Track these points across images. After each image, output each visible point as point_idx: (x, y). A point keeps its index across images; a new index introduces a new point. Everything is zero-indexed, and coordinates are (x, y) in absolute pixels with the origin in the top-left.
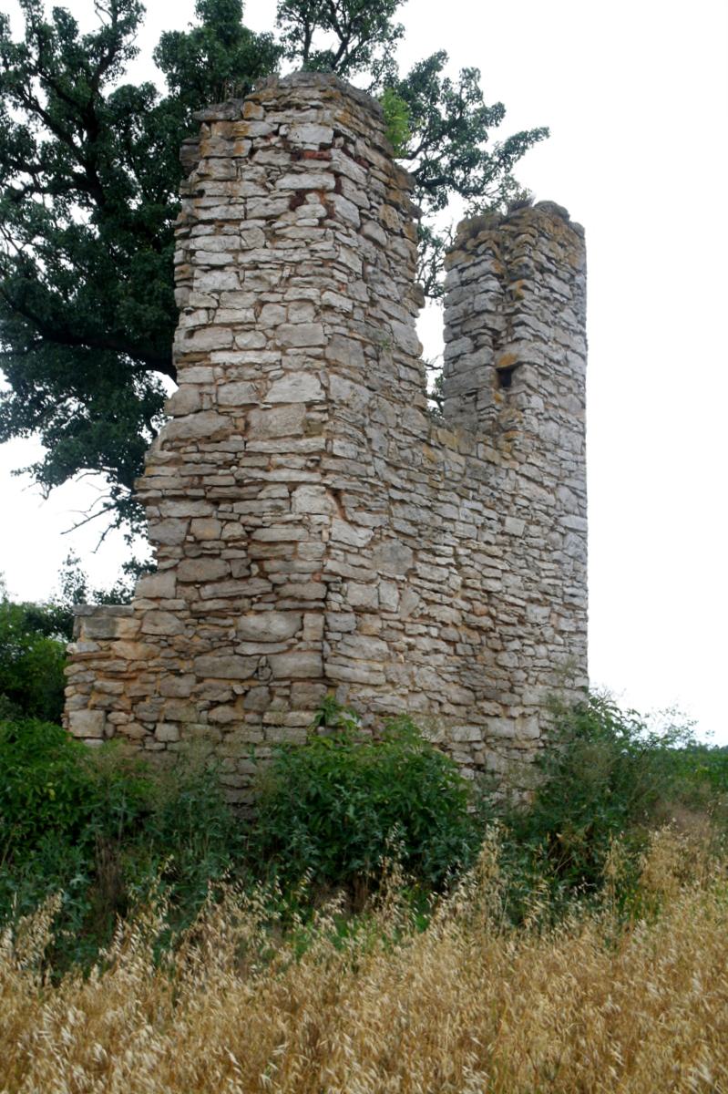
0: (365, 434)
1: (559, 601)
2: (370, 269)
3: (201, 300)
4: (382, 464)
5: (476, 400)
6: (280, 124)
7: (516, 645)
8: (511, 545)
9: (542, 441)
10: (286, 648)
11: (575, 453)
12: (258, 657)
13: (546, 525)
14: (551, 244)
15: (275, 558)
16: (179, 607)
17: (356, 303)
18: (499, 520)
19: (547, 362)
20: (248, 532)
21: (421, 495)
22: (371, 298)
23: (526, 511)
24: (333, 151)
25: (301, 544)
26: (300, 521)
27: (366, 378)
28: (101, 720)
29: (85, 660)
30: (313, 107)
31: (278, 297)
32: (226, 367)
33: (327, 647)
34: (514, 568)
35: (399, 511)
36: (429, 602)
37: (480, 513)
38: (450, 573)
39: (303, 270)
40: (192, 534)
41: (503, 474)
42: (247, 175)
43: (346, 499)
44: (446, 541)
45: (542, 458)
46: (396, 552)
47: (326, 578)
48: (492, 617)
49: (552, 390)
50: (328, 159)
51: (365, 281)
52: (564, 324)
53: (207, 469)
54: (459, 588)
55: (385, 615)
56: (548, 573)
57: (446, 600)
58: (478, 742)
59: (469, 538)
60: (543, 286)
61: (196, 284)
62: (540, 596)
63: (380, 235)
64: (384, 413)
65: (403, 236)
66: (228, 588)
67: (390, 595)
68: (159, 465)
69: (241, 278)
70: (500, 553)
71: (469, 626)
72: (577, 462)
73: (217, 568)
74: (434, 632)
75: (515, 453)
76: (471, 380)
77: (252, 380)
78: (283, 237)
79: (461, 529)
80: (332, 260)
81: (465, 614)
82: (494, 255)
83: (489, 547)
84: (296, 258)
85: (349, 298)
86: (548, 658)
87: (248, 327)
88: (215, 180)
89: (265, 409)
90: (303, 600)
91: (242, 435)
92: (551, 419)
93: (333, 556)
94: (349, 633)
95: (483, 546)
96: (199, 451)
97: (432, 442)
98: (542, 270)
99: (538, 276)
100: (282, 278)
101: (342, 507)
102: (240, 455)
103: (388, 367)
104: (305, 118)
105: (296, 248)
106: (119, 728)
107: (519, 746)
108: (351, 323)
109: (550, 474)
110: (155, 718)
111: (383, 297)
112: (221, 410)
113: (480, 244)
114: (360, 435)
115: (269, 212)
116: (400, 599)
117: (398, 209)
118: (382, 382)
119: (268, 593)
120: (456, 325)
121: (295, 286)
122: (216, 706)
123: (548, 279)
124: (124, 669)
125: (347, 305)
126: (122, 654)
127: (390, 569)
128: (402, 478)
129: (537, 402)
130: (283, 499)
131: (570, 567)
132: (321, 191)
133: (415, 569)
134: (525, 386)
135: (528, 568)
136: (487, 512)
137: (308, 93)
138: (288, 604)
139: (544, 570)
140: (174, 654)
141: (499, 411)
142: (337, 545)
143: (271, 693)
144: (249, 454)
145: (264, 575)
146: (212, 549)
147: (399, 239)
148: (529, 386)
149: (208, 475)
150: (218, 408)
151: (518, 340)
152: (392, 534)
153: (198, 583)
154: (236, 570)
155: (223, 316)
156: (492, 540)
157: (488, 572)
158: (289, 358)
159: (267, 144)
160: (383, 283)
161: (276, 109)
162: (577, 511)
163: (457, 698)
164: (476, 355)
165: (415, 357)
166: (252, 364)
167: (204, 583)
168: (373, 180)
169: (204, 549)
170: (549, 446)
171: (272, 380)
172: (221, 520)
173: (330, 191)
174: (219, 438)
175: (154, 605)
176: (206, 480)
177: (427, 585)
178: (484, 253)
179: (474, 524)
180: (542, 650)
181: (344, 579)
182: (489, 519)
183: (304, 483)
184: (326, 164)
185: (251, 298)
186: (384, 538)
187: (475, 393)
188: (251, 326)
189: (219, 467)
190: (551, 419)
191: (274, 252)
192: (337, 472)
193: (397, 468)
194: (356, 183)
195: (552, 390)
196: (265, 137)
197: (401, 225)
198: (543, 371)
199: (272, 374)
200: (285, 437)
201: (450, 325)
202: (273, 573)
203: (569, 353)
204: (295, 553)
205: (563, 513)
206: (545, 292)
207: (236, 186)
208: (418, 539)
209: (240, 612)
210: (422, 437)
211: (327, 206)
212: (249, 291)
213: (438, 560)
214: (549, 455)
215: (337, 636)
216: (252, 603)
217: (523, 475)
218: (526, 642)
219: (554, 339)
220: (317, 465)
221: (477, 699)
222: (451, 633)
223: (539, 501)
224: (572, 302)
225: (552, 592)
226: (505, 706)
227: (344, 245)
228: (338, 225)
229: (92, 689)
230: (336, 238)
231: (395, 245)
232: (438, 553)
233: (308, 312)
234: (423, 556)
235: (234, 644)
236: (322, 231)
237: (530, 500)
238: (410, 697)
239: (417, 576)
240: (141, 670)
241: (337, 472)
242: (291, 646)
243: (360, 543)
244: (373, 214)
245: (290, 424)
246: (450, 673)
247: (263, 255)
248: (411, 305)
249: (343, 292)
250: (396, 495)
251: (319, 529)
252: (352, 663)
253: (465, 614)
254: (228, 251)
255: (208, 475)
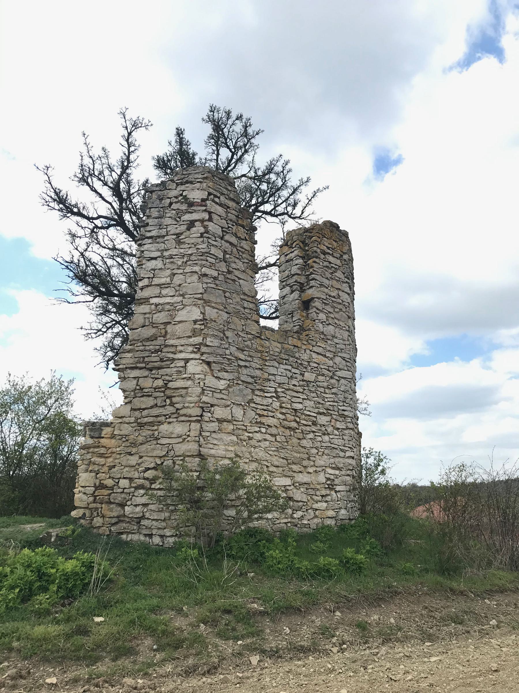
0: (224, 334)
1: (336, 413)
2: (228, 256)
3: (146, 274)
4: (235, 348)
5: (292, 317)
6: (183, 191)
7: (311, 436)
8: (308, 386)
9: (325, 335)
10: (182, 440)
11: (344, 340)
12: (168, 445)
13: (328, 376)
14: (329, 241)
15: (178, 396)
16: (131, 421)
17: (220, 273)
18: (301, 374)
19: (328, 297)
20: (166, 384)
21: (256, 363)
22: (228, 270)
23: (316, 369)
24: (207, 202)
25: (190, 389)
26: (190, 377)
27: (225, 308)
28: (94, 478)
29: (88, 448)
30: (198, 182)
31: (181, 271)
32: (156, 305)
33: (201, 439)
34: (309, 397)
35: (245, 371)
36: (260, 416)
37: (290, 371)
38: (273, 400)
39: (193, 258)
40: (139, 386)
41: (303, 352)
42: (168, 215)
43: (214, 366)
44: (270, 385)
45: (325, 343)
46: (242, 392)
47: (201, 405)
48: (297, 422)
49: (331, 310)
50: (206, 206)
51: (226, 262)
52: (337, 278)
53: (147, 354)
54: (278, 408)
55: (235, 423)
56: (329, 399)
57: (270, 414)
58: (290, 486)
59: (283, 383)
60: (325, 261)
61: (144, 266)
62: (325, 411)
63: (233, 240)
64: (235, 324)
65: (246, 240)
66: (156, 411)
67: (238, 413)
68: (125, 353)
69: (165, 263)
70: (301, 390)
71: (284, 427)
72: (345, 345)
73: (150, 401)
74: (263, 430)
75: (310, 341)
76: (290, 307)
77: (168, 311)
78: (184, 243)
79: (278, 379)
80: (206, 253)
81: (281, 421)
82: (300, 248)
83: (295, 388)
84: (190, 252)
85: (216, 270)
86: (330, 442)
87: (167, 286)
88: (153, 218)
89: (174, 324)
90: (190, 416)
91: (164, 337)
92: (330, 324)
93: (206, 394)
94: (214, 432)
95: (292, 387)
96: (143, 346)
97: (263, 337)
98: (324, 253)
99: (322, 256)
100: (183, 262)
101: (212, 370)
102: (162, 347)
103: (237, 302)
104: (195, 187)
105: (190, 248)
106: (102, 482)
107: (313, 487)
108: (217, 282)
109: (329, 351)
110: (119, 477)
111: (235, 269)
112: (154, 325)
113: (294, 242)
114: (222, 335)
115: (178, 232)
116: (244, 414)
117: (244, 228)
118: (234, 310)
119: (174, 413)
120: (284, 281)
121: (190, 265)
122: (148, 470)
123: (328, 258)
124: (105, 452)
125: (215, 274)
126: (105, 445)
127: (239, 400)
128: (245, 355)
129: (322, 316)
130: (182, 367)
131: (342, 396)
132: (202, 221)
133: (253, 399)
134: (315, 309)
135: (318, 397)
136: (293, 370)
137: (197, 176)
138: (183, 418)
139: (327, 398)
140: (129, 444)
141: (303, 321)
142: (208, 389)
143: (174, 463)
144: (166, 346)
145: (172, 404)
146: (148, 392)
147: (244, 242)
148: (317, 309)
149: (147, 357)
150: (153, 325)
151: (312, 287)
152: (240, 382)
153: (142, 409)
154: (159, 402)
155: (156, 281)
156: (297, 384)
157: (294, 400)
158: (186, 300)
159: (177, 200)
160: (235, 262)
161: (182, 184)
162: (346, 368)
163: (276, 463)
164: (293, 295)
165: (253, 297)
166: (169, 303)
167: (144, 409)
168: (229, 214)
169: (144, 392)
170: (329, 337)
171: (178, 311)
172: (153, 378)
173: (206, 221)
174: (153, 339)
175: (120, 420)
176: (146, 359)
177: (260, 407)
178: (295, 247)
179: (286, 376)
180: (326, 438)
181: (212, 406)
182: (295, 374)
183: (192, 359)
184: (204, 208)
185: (168, 272)
186: (235, 385)
187: (292, 313)
188: (169, 285)
189: (152, 353)
190: (330, 324)
191: (180, 250)
192: (208, 353)
193: (243, 351)
194: (220, 216)
195: (331, 310)
196: (176, 197)
197: (245, 235)
198: (325, 301)
199: (178, 307)
200: (184, 337)
201: (281, 281)
202: (177, 403)
203: (340, 292)
204: (187, 393)
205: (338, 369)
206: (326, 264)
207: (163, 220)
208: (255, 384)
209: (161, 423)
210: (257, 335)
211: (205, 227)
212: (168, 269)
213: (266, 394)
214: (329, 342)
215: (208, 434)
216: (167, 418)
217: (314, 352)
218: (317, 434)
219: (332, 286)
220: (199, 350)
221: (288, 464)
222: (274, 431)
223: (324, 364)
224: (341, 268)
225: (331, 409)
226: (305, 467)
227: (213, 245)
228: (210, 236)
229: (90, 463)
230: (208, 242)
231: (242, 245)
232: (265, 391)
233: (195, 277)
234: (257, 393)
235: (157, 439)
236: (202, 239)
237: (319, 364)
238: (250, 463)
239: (254, 403)
240: (112, 453)
241: (208, 353)
242: (185, 439)
243: (221, 388)
244: (229, 230)
245: (186, 331)
246: (273, 451)
247: (174, 252)
248: (250, 272)
249: (213, 267)
250: (242, 363)
251: (199, 381)
252: (216, 447)
253: (281, 421)
254: (158, 250)
255: (147, 357)
